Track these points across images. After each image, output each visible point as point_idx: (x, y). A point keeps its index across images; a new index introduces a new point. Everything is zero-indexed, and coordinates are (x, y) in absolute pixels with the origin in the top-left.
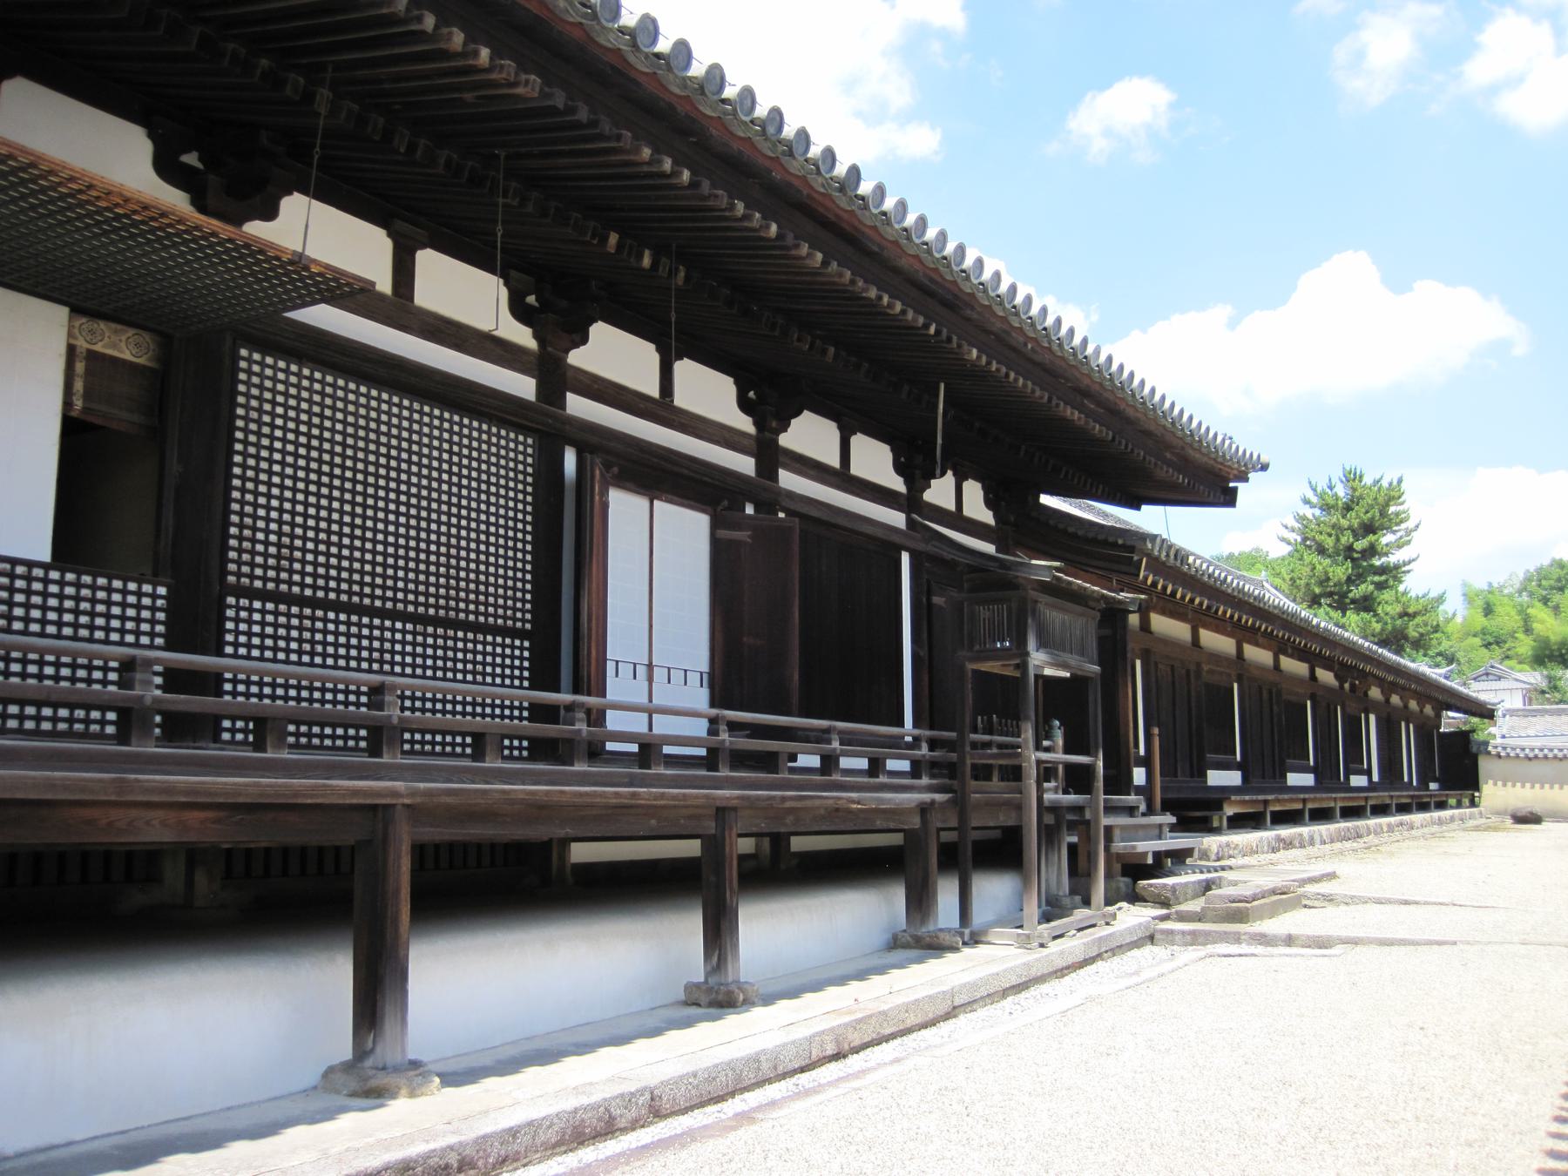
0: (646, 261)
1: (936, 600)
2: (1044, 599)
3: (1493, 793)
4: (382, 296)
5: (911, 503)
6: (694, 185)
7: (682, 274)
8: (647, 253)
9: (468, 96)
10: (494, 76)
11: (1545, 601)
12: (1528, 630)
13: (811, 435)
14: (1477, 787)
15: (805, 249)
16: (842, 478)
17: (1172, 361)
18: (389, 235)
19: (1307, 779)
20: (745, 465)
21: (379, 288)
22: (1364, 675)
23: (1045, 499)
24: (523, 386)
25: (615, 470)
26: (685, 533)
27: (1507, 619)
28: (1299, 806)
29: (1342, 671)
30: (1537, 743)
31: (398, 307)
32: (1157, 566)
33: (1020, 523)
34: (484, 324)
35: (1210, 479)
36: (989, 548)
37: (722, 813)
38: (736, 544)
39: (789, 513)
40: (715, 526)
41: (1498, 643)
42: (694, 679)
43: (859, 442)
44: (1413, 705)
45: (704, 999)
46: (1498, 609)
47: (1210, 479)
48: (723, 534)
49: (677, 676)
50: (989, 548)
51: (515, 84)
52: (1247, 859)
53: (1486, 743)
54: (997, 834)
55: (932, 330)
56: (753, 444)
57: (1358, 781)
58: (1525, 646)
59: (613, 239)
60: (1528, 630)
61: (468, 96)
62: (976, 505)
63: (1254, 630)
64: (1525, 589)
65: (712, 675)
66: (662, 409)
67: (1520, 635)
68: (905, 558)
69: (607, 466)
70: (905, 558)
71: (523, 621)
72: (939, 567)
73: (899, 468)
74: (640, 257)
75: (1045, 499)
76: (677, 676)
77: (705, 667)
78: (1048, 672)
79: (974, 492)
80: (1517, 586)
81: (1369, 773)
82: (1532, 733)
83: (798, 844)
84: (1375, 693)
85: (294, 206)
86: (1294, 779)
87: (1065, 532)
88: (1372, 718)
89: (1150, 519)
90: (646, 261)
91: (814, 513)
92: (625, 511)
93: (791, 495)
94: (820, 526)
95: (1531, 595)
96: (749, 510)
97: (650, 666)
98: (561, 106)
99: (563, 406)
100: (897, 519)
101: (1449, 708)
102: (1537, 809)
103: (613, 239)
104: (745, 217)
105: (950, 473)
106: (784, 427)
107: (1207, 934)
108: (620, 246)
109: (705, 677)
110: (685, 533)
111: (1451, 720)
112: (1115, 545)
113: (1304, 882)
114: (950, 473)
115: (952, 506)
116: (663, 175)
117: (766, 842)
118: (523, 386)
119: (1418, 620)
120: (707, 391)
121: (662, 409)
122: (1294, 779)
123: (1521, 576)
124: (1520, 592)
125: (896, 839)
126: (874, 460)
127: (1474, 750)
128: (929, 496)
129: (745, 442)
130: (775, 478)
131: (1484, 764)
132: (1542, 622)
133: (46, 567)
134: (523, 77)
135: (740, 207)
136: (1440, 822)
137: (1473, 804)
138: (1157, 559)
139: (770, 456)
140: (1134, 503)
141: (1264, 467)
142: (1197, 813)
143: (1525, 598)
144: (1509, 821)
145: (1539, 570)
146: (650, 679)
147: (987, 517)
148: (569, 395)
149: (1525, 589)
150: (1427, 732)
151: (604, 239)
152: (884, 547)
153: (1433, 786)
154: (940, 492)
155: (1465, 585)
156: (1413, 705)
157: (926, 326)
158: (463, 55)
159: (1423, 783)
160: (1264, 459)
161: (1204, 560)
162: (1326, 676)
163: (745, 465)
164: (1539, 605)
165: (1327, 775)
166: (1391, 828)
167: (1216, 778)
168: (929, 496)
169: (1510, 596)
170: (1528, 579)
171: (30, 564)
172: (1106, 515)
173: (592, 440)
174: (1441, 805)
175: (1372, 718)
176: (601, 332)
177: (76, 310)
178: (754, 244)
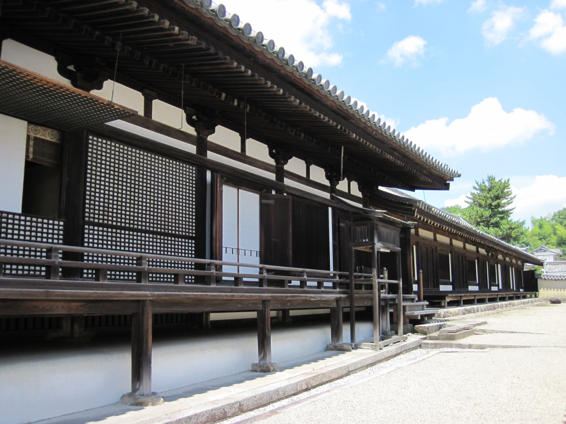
0: (236, 103)
1: (342, 225)
2: (380, 224)
3: (543, 292)
4: (140, 117)
5: (332, 190)
6: (252, 75)
7: (248, 108)
8: (236, 100)
9: (171, 44)
10: (180, 37)
11: (561, 223)
12: (555, 234)
13: (296, 165)
14: (537, 291)
15: (293, 98)
16: (307, 181)
17: (426, 138)
18: (56, 59)
19: (476, 288)
20: (272, 176)
21: (139, 113)
22: (496, 250)
23: (380, 188)
24: (191, 149)
25: (225, 178)
26: (251, 201)
27: (547, 229)
28: (473, 298)
29: (488, 249)
30: (559, 274)
31: (146, 121)
32: (421, 212)
33: (372, 197)
34: (177, 127)
35: (439, 180)
36: (360, 206)
37: (265, 302)
38: (268, 205)
39: (288, 193)
40: (261, 198)
41: (544, 238)
42: (254, 254)
43: (313, 168)
44: (514, 261)
45: (258, 369)
46: (545, 226)
47: (439, 180)
48: (264, 201)
49: (248, 253)
50: (360, 206)
51: (188, 40)
52: (454, 317)
53: (540, 275)
54: (364, 309)
55: (339, 127)
56: (275, 169)
57: (494, 288)
58: (554, 239)
59: (224, 95)
60: (555, 234)
61: (171, 44)
62: (355, 190)
63: (456, 234)
64: (554, 219)
65: (260, 252)
66: (242, 157)
67: (552, 236)
68: (330, 209)
69: (222, 177)
70: (330, 209)
71: (192, 233)
72: (342, 213)
73: (328, 177)
74: (233, 102)
75: (380, 188)
76: (248, 253)
77: (258, 250)
78: (382, 250)
79: (354, 185)
80: (551, 218)
81: (498, 286)
82: (557, 271)
83: (292, 313)
84: (500, 257)
85: (109, 84)
86: (471, 288)
87: (388, 200)
88: (499, 266)
89: (418, 195)
90: (236, 103)
91: (297, 194)
92: (229, 193)
93: (288, 187)
94: (300, 199)
95: (556, 221)
96: (274, 192)
97: (238, 249)
98: (204, 48)
99: (206, 156)
100: (327, 195)
101: (527, 262)
102: (559, 298)
103: (224, 95)
104: (271, 87)
105: (346, 179)
106: (286, 163)
107: (440, 344)
108: (226, 98)
109: (258, 253)
110: (251, 201)
111: (528, 267)
112: (405, 204)
113: (475, 325)
114: (346, 179)
115: (347, 191)
116: (241, 72)
117: (281, 312)
118: (191, 149)
119: (515, 230)
120: (258, 150)
121: (242, 157)
122: (471, 288)
123: (553, 214)
124: (552, 220)
125: (327, 311)
126: (318, 174)
127: (536, 277)
128: (338, 187)
129: (272, 168)
130: (283, 181)
131: (539, 282)
132: (560, 231)
133: (20, 215)
134: (191, 37)
135: (269, 83)
136: (524, 303)
137: (536, 297)
138: (421, 209)
139: (281, 173)
140: (412, 189)
141: (459, 176)
142: (436, 300)
143: (554, 222)
144: (549, 303)
145: (559, 212)
146: (238, 254)
147: (360, 195)
148: (208, 152)
149: (554, 219)
150: (519, 271)
151: (221, 95)
152: (322, 206)
153: (521, 290)
154: (342, 185)
155: (532, 217)
156: (514, 261)
157: (337, 126)
158: (169, 29)
159: (518, 289)
160: (459, 173)
161: (438, 209)
162: (482, 251)
163: (272, 176)
164: (559, 224)
165: (483, 286)
166: (506, 306)
167: (443, 288)
168: (338, 187)
169: (548, 221)
170: (555, 215)
171: (14, 214)
172: (402, 193)
173: (217, 168)
174: (524, 297)
175: (499, 266)
176: (219, 129)
177: (30, 122)
178: (275, 96)
